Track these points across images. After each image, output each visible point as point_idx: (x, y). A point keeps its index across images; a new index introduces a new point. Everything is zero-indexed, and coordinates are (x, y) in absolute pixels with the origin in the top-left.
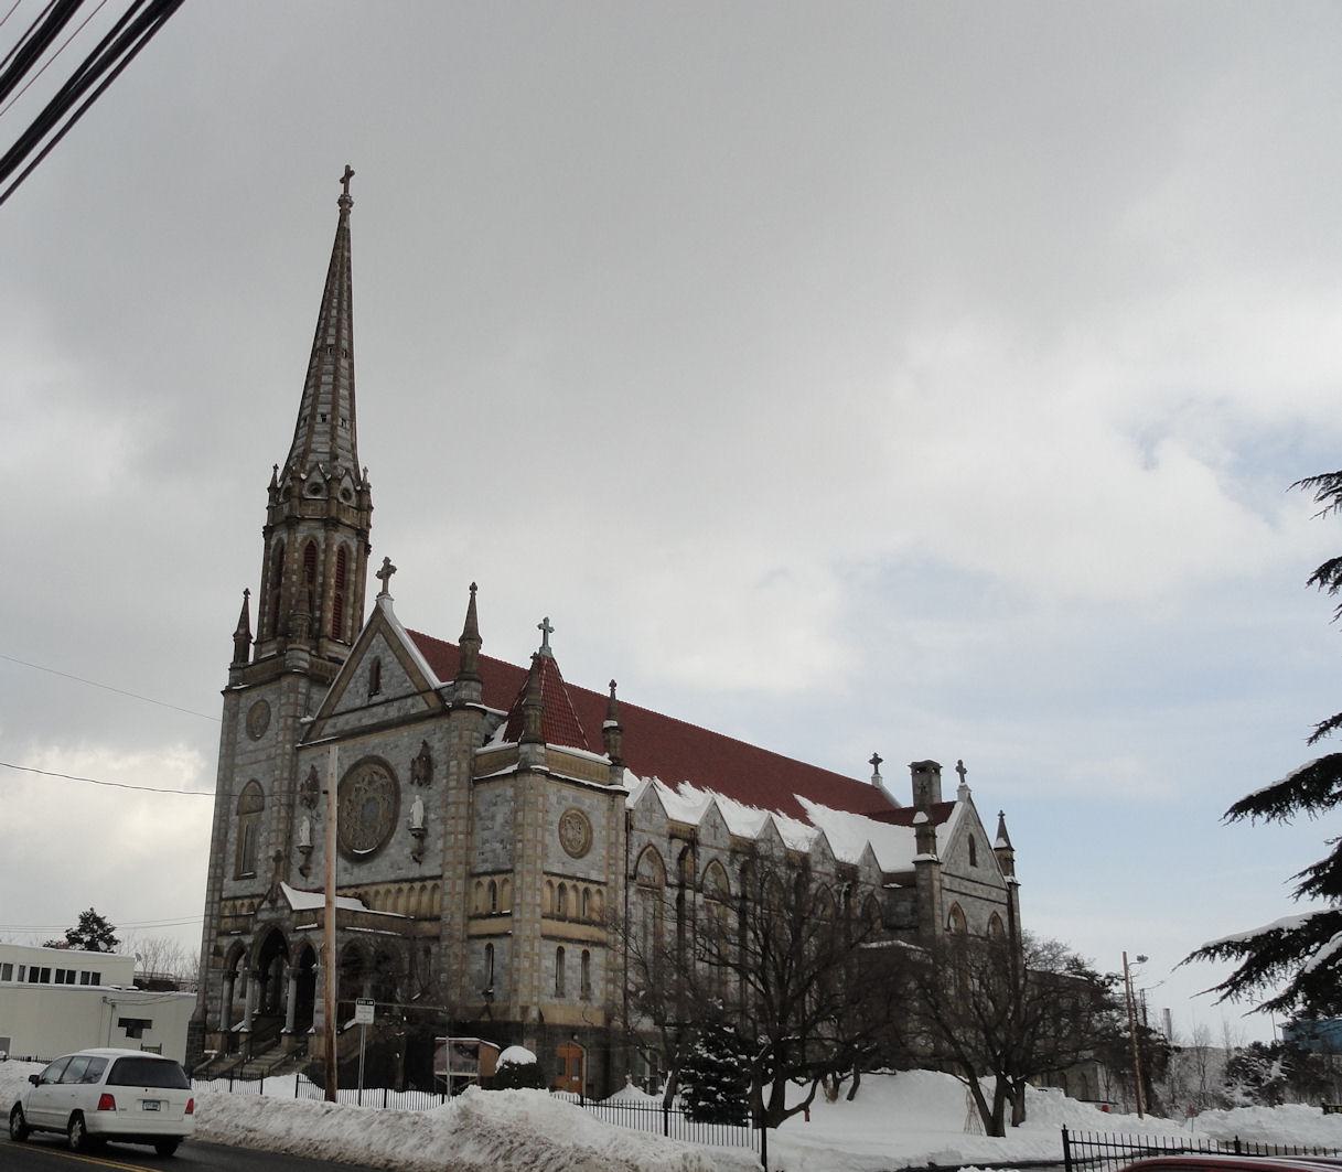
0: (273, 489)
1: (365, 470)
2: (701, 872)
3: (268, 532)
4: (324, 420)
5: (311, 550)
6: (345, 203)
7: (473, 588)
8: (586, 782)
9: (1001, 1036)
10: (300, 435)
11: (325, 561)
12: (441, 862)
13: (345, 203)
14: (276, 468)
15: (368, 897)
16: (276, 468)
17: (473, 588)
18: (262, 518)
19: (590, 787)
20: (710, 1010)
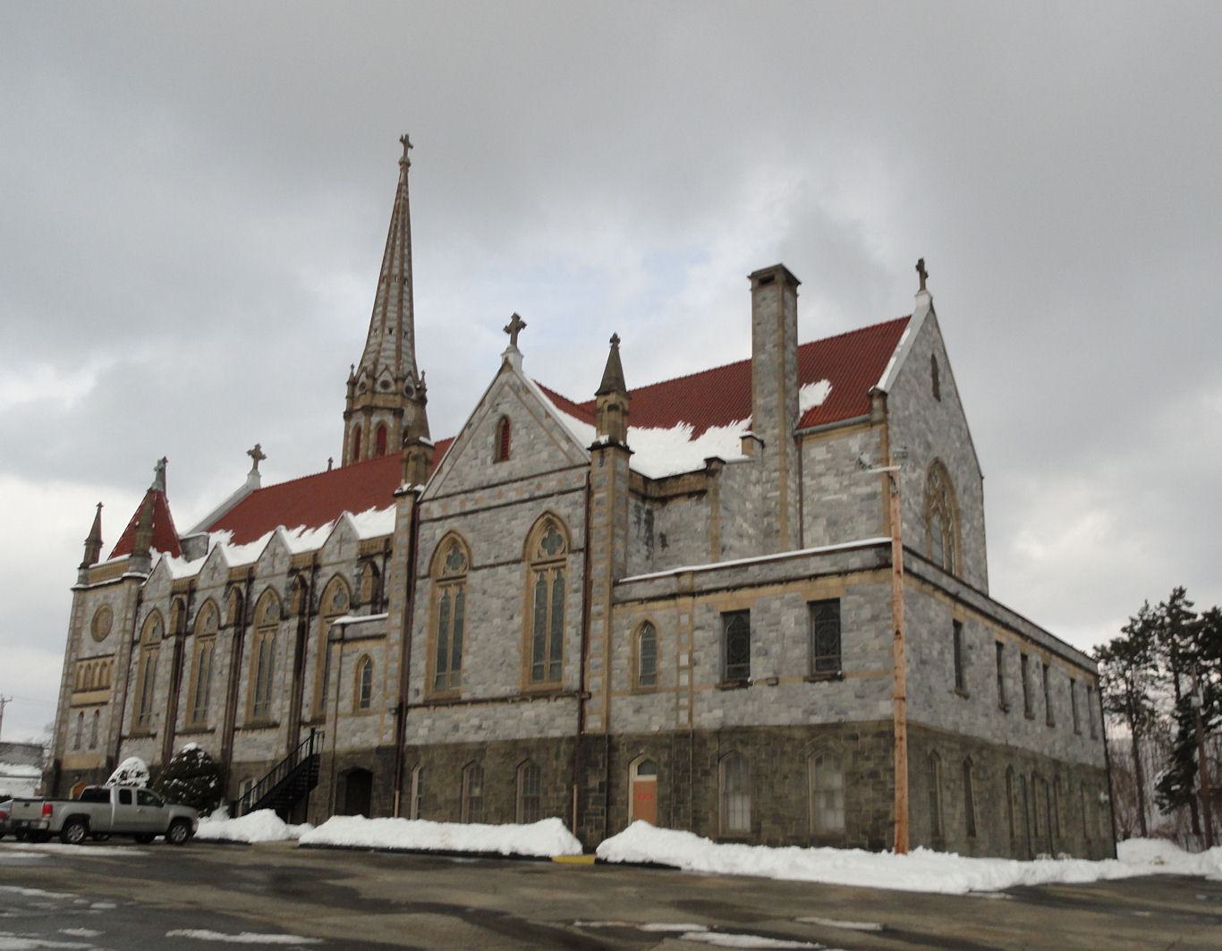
0: (353, 383)
1: (423, 373)
2: (195, 615)
3: (348, 415)
4: (391, 332)
5: (382, 430)
6: (405, 164)
7: (100, 506)
8: (107, 582)
9: (1103, 797)
10: (371, 343)
11: (785, 376)
12: (696, 669)
13: (405, 164)
14: (353, 367)
15: (620, 698)
16: (353, 367)
17: (100, 506)
18: (343, 406)
19: (110, 584)
20: (890, 786)
